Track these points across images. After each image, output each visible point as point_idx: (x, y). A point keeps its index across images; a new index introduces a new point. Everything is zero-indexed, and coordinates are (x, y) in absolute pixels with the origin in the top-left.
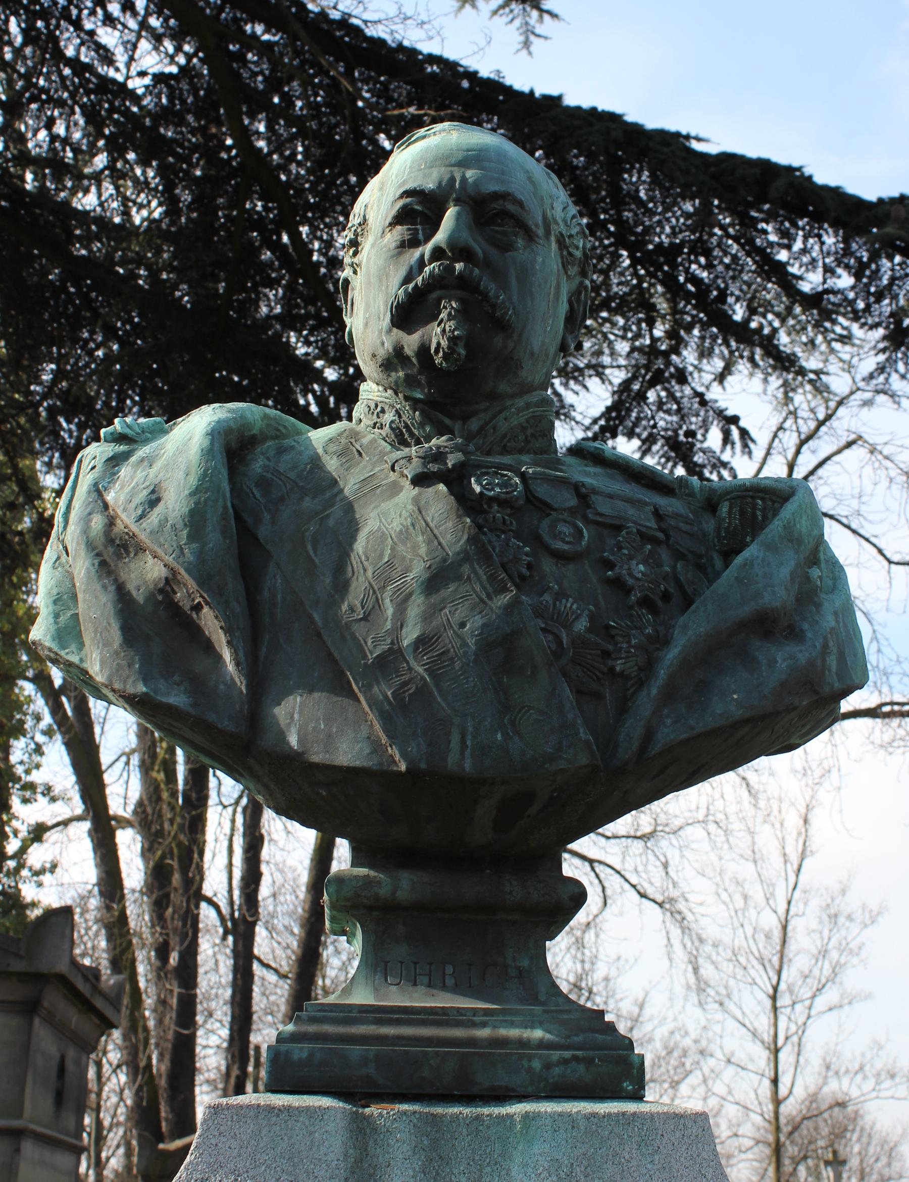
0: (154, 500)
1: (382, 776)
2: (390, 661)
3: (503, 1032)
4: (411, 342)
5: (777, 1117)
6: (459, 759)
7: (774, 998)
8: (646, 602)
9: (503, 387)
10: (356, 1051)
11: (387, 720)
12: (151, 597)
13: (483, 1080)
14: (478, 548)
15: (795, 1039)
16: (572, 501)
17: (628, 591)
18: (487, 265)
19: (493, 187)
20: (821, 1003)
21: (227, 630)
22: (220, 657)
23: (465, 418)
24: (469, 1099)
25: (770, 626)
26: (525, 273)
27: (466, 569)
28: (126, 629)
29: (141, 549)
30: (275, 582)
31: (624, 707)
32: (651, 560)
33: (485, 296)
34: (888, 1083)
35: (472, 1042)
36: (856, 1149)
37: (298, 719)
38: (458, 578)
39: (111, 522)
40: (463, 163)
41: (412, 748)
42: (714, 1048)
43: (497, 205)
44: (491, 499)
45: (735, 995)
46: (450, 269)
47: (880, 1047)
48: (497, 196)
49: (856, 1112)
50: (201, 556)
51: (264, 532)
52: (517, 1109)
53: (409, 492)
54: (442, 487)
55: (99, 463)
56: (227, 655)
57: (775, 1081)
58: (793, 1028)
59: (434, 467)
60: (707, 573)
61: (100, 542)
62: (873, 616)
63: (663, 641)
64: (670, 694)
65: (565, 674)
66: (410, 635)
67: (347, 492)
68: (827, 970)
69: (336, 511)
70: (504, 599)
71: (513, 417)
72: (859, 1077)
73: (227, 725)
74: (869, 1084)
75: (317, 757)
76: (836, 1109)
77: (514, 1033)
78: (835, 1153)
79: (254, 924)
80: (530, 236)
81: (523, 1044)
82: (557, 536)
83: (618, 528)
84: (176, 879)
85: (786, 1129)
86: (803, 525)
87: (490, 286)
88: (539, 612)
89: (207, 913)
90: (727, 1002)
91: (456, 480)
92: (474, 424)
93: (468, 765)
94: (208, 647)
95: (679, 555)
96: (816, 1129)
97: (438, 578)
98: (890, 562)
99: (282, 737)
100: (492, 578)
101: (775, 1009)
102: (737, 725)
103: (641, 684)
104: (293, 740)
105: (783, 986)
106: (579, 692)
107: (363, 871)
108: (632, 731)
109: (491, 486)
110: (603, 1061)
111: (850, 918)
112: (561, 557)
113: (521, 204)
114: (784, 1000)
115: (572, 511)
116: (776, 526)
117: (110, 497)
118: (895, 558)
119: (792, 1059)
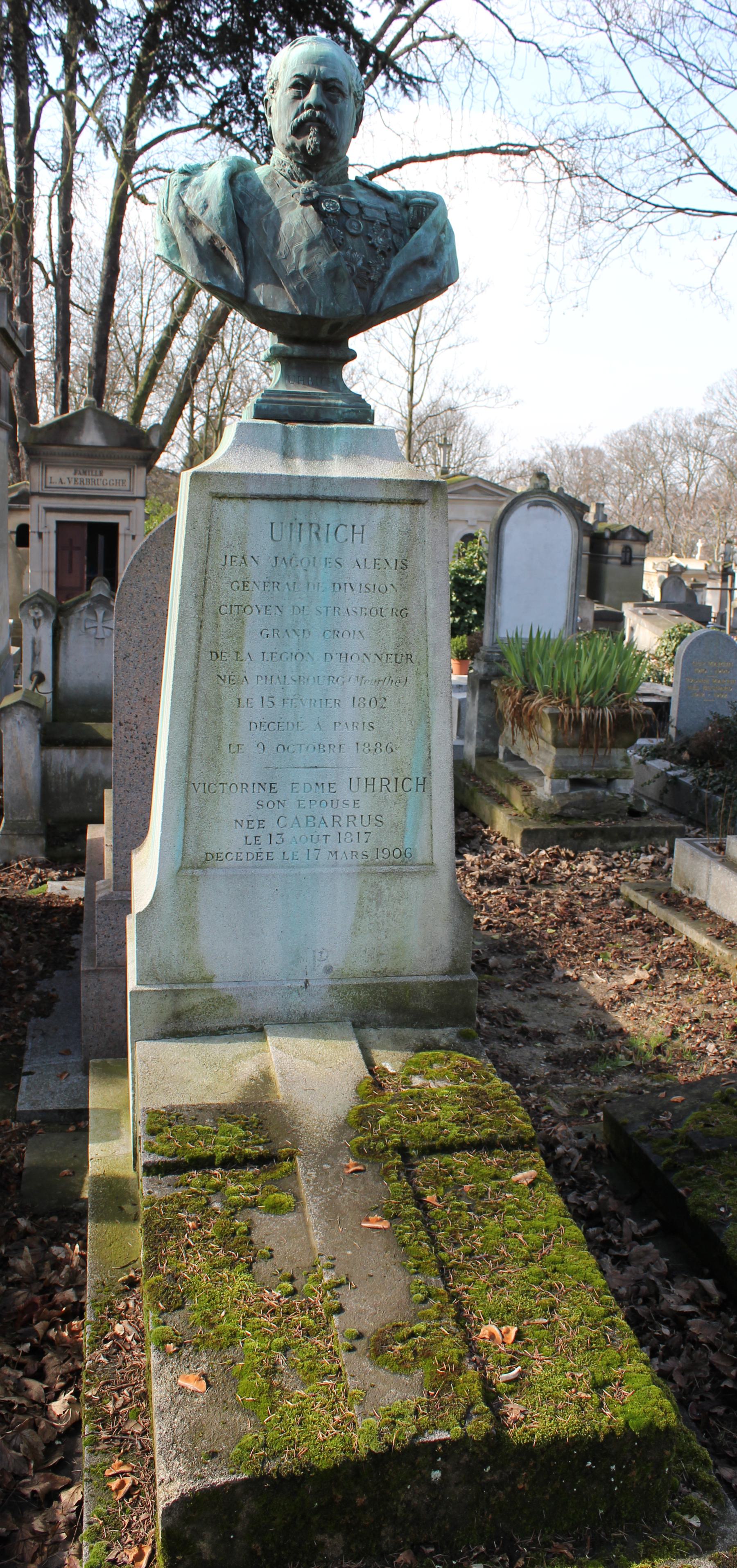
0: (206, 207)
1: (294, 317)
2: (295, 275)
3: (330, 401)
4: (298, 143)
5: (411, 416)
6: (319, 312)
7: (414, 338)
8: (382, 253)
9: (332, 160)
10: (282, 406)
11: (294, 296)
12: (206, 243)
13: (323, 416)
14: (325, 234)
15: (426, 366)
16: (357, 211)
17: (376, 249)
18: (328, 111)
19: (331, 76)
20: (444, 343)
21: (237, 260)
22: (232, 268)
23: (317, 171)
24: (318, 422)
25: (425, 262)
26: (342, 113)
27: (321, 242)
28: (200, 257)
29: (200, 222)
30: (251, 241)
31: (373, 292)
32: (385, 236)
33: (327, 126)
34: (483, 397)
35: (319, 404)
36: (460, 438)
37: (262, 293)
38: (318, 245)
39: (187, 211)
40: (319, 63)
41: (303, 307)
42: (372, 369)
43: (332, 84)
44: (331, 213)
45: (388, 336)
46: (314, 114)
47: (480, 374)
48: (332, 80)
49: (462, 414)
50: (226, 231)
51: (246, 219)
52: (334, 426)
53: (299, 208)
54: (311, 207)
55: (178, 183)
56: (236, 269)
57: (411, 392)
58: (425, 359)
59: (308, 198)
60: (405, 238)
61: (184, 219)
62: (500, 81)
63: (387, 268)
64: (389, 288)
65: (354, 281)
66: (302, 265)
67: (276, 204)
68: (450, 322)
69: (272, 213)
70: (334, 254)
71: (334, 172)
72: (466, 391)
73: (238, 294)
74: (472, 397)
75: (270, 308)
76: (449, 412)
77: (333, 401)
78: (445, 439)
79: (70, 278)
80: (343, 95)
81: (336, 405)
82: (352, 227)
83: (373, 222)
84: (15, 246)
85: (416, 423)
86: (440, 220)
87: (329, 121)
88: (346, 258)
89: (36, 271)
90: (382, 339)
91: (316, 203)
92: (320, 174)
93: (322, 314)
94: (228, 263)
95: (394, 231)
96: (436, 422)
97: (311, 245)
98: (516, 39)
99: (257, 300)
100: (330, 246)
101: (414, 345)
102: (411, 300)
103: (379, 284)
104: (261, 301)
105: (420, 331)
106: (359, 288)
107: (282, 345)
108: (376, 302)
109: (329, 207)
110: (361, 412)
111: (467, 287)
112: (353, 236)
113: (341, 83)
114: (420, 340)
115: (357, 216)
116: (429, 221)
117: (185, 199)
118: (519, 37)
119: (423, 378)
